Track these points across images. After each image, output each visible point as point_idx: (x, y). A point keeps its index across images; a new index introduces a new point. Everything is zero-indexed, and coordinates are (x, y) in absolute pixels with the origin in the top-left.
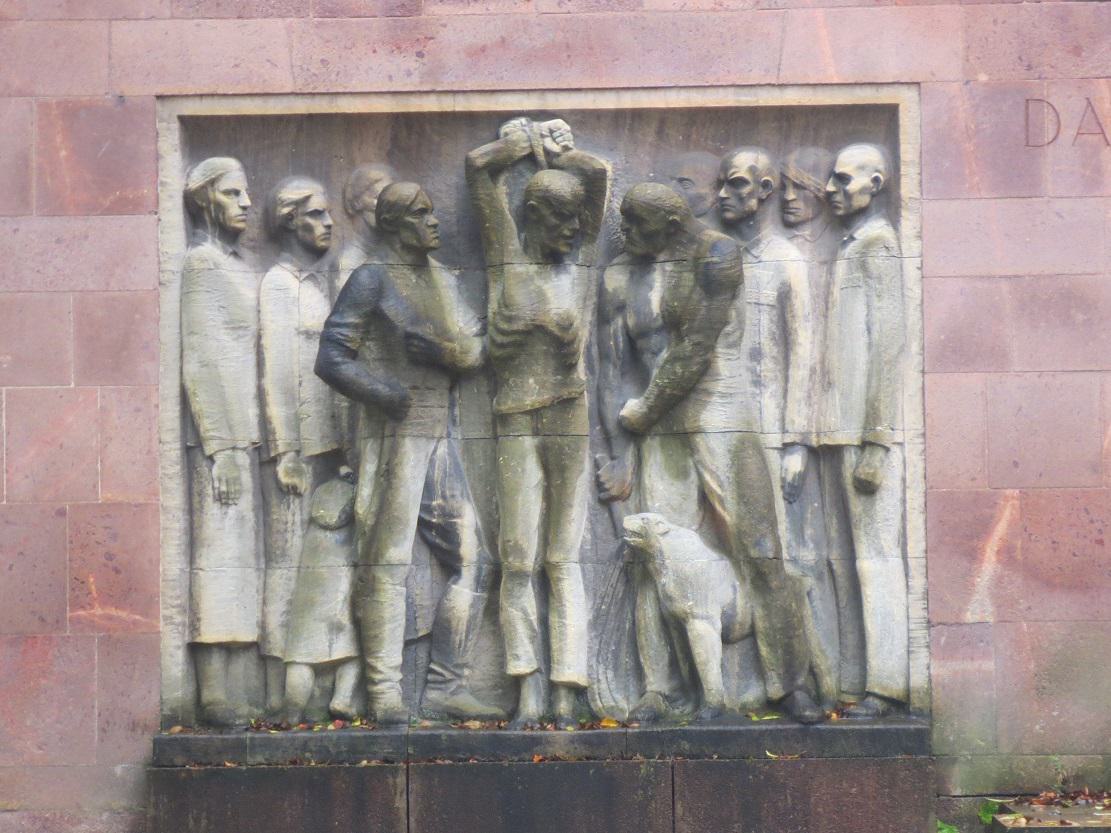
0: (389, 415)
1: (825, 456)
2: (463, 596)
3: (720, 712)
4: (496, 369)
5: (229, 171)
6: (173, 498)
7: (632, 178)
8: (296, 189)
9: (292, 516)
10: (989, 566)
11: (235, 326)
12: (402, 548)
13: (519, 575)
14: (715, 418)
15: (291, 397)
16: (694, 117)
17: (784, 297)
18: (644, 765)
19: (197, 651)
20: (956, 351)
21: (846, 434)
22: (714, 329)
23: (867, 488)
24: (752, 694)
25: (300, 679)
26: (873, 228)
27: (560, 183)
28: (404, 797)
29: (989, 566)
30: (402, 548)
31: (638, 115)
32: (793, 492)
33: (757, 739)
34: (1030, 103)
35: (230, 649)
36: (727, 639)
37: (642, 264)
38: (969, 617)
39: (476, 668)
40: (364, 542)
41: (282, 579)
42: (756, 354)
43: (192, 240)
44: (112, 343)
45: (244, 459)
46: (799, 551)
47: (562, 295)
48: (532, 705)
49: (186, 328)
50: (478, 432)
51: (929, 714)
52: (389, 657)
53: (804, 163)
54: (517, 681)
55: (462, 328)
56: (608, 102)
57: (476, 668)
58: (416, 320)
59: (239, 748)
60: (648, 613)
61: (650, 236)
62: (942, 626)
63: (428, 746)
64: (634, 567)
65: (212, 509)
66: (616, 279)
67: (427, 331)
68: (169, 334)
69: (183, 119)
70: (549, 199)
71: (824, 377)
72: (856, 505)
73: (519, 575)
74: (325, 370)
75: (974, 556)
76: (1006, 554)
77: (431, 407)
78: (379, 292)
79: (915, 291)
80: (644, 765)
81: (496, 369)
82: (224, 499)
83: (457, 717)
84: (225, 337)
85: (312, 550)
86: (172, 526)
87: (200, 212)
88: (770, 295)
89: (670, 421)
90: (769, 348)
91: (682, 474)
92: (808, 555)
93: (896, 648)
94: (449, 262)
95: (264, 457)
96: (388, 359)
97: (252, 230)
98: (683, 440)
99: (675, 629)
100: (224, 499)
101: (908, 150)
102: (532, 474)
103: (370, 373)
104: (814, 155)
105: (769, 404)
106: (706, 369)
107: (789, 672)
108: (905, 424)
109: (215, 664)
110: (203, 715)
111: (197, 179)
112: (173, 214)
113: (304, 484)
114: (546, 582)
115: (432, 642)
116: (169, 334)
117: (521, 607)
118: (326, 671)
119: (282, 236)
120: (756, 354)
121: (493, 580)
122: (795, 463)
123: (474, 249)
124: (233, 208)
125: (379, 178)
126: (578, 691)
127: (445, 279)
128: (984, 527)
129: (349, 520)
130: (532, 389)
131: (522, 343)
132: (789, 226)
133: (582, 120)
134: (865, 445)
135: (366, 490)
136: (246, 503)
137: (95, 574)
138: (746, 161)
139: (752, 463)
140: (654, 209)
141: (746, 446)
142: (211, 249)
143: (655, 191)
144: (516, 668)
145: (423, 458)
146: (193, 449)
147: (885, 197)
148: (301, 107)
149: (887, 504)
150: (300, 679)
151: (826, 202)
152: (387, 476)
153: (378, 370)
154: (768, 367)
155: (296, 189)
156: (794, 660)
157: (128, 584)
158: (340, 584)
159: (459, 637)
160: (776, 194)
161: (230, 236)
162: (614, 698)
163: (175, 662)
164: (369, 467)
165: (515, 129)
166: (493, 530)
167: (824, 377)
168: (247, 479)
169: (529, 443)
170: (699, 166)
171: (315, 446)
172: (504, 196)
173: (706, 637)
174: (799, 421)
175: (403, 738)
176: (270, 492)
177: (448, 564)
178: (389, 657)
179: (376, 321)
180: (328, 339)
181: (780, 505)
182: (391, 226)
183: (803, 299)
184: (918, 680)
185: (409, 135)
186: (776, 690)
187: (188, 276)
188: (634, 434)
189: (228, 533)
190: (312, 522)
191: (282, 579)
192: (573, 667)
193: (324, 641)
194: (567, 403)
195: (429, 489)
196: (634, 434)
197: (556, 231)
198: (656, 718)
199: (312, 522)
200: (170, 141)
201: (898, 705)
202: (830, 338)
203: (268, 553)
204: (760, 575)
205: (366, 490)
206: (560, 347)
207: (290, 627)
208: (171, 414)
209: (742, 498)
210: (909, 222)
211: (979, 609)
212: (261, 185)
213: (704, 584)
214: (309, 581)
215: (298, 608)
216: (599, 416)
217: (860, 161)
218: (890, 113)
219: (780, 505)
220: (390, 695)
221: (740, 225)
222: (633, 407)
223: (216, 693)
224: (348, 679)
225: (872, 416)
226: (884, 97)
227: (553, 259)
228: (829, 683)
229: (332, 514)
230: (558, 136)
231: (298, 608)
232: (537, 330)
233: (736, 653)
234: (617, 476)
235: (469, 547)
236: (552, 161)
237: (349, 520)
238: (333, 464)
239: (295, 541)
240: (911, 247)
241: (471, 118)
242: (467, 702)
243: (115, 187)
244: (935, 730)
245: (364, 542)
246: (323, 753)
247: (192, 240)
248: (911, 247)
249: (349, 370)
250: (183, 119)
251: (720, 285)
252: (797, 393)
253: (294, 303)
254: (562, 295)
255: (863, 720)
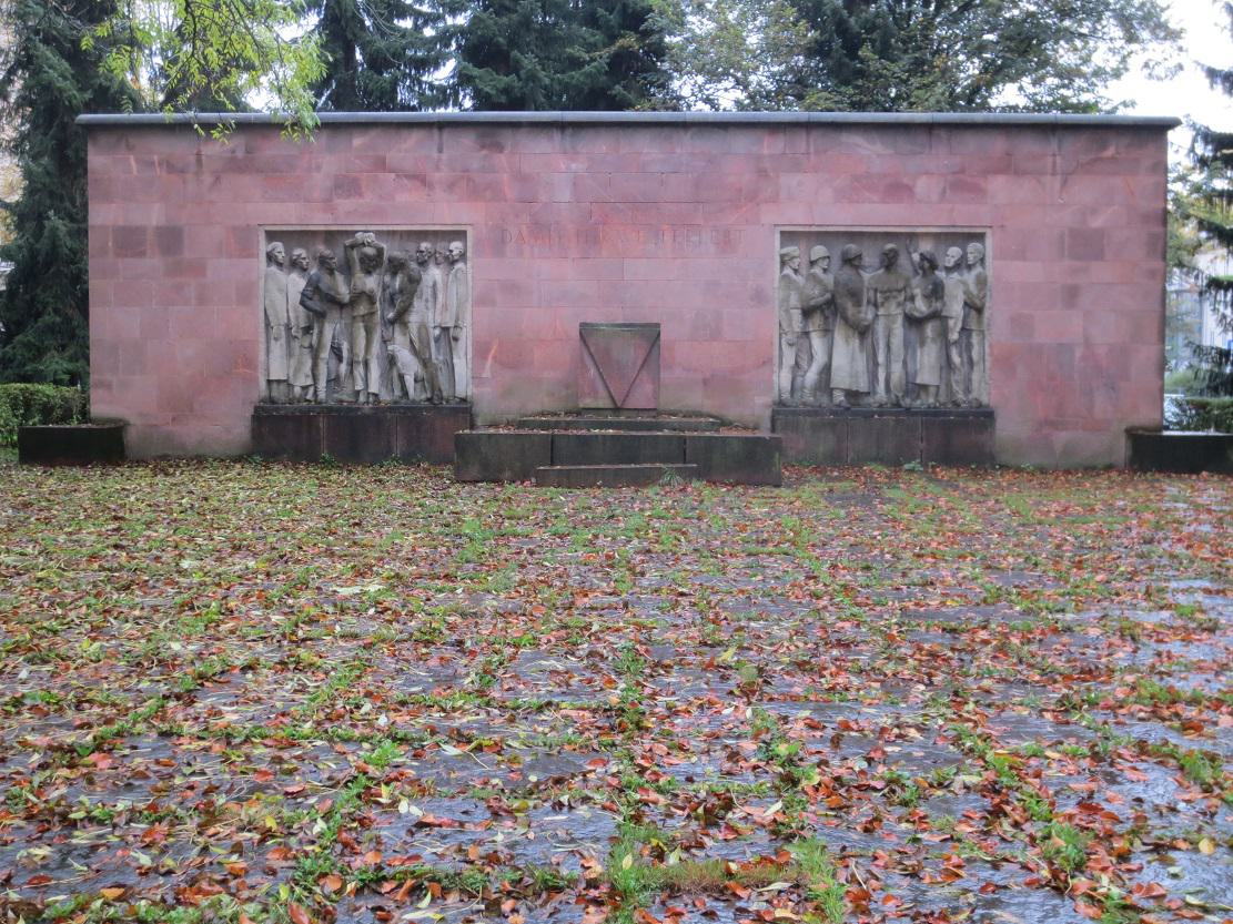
0: (321, 316)
1: (445, 330)
2: (343, 368)
3: (414, 401)
4: (353, 303)
5: (279, 246)
6: (262, 339)
7: (391, 250)
8: (298, 251)
9: (296, 345)
10: (490, 360)
11: (280, 290)
12: (325, 354)
13: (358, 362)
14: (413, 319)
15: (295, 311)
16: (410, 234)
17: (435, 284)
18: (389, 415)
19: (269, 382)
20: (482, 301)
21: (451, 324)
22: (412, 294)
23: (456, 339)
24: (423, 397)
25: (297, 390)
26: (460, 265)
27: (370, 251)
28: (322, 423)
29: (490, 360)
30: (325, 354)
31: (394, 232)
32: (437, 340)
33: (421, 409)
34: (503, 231)
35: (279, 382)
36: (416, 381)
37: (394, 274)
38: (484, 375)
39: (348, 389)
40: (315, 352)
41: (293, 362)
42: (427, 301)
43: (268, 266)
44: (246, 294)
45: (283, 328)
46: (437, 356)
47: (371, 283)
48: (362, 398)
49: (266, 291)
50: (348, 321)
51: (472, 403)
52: (322, 384)
53: (441, 246)
54: (358, 392)
55: (344, 292)
56: (385, 228)
57: (348, 389)
58: (330, 289)
59: (277, 409)
60: (395, 374)
61: (396, 267)
62: (476, 378)
63: (330, 409)
64: (391, 361)
65: (273, 342)
66: (387, 278)
67: (332, 293)
68: (261, 293)
69: (267, 232)
70: (366, 255)
71: (445, 307)
72: (453, 343)
73: (358, 362)
74: (302, 303)
75: (486, 358)
76: (494, 358)
77: (334, 314)
78: (318, 281)
79: (470, 284)
80: (389, 415)
81: (353, 303)
82: (276, 339)
83: (341, 401)
84: (277, 294)
85: (301, 354)
86: (262, 347)
87: (271, 258)
88: (431, 284)
89: (400, 319)
90: (430, 299)
91: (405, 335)
92: (441, 358)
93: (463, 385)
94: (342, 273)
95: (288, 328)
96: (321, 300)
97: (287, 263)
98: (405, 325)
99: (401, 377)
100: (276, 339)
101: (469, 244)
102: (362, 333)
103: (316, 304)
104: (444, 244)
105: (430, 315)
106: (411, 304)
107: (433, 392)
108: (467, 322)
109: (275, 385)
110: (272, 401)
111: (270, 248)
112: (263, 258)
113: (299, 335)
114: (366, 364)
115: (334, 381)
116: (261, 293)
117: (359, 371)
118: (305, 388)
119: (295, 265)
120: (427, 301)
121: (351, 364)
122: (437, 332)
123: (347, 269)
124: (280, 257)
125: (322, 249)
126: (376, 395)
127: (340, 278)
128: (488, 351)
129: (311, 346)
130: (362, 309)
131: (360, 296)
132: (438, 264)
133: (378, 233)
134: (456, 327)
135: (315, 337)
136: (283, 340)
137: (241, 360)
138: (424, 245)
139: (423, 331)
140: (395, 259)
141: (423, 327)
142: (274, 268)
143: (397, 254)
144: (358, 388)
145: (330, 329)
146: (268, 325)
147: (463, 256)
148: (299, 228)
149: (461, 343)
150: (297, 390)
151: (447, 258)
152: (321, 332)
153: (319, 303)
154: (430, 304)
155: (298, 251)
156: (434, 387)
157: (250, 363)
158: (309, 363)
159: (342, 379)
160: (433, 255)
161: (280, 265)
162: (385, 397)
163: (263, 384)
164: (316, 331)
165: (359, 235)
166: (351, 350)
167: (445, 307)
168: (283, 333)
169: (361, 324)
170: (411, 247)
171: (303, 325)
172: (355, 254)
173: (410, 381)
174: (438, 320)
175: (399, 446)
176: (290, 338)
177: (340, 359)
178: (322, 384)
179: (317, 289)
180: (303, 294)
181: (433, 344)
182: (323, 262)
183: (440, 285)
184: (469, 393)
185: (330, 236)
186: (429, 395)
187: (267, 276)
188: (392, 322)
189: (278, 349)
190: (301, 346)
191: (293, 362)
192: (374, 388)
193: (304, 380)
194: (373, 314)
195: (334, 338)
196: (392, 322)
197: (371, 264)
198: (396, 402)
199: (301, 346)
200: (262, 237)
201: (464, 400)
202: (446, 296)
203: (290, 354)
204: (425, 363)
205: (315, 337)
206: (371, 299)
207: (294, 375)
208: (262, 314)
209: (421, 341)
210: (469, 264)
211: (487, 374)
212: (288, 251)
213: (409, 364)
214: (300, 363)
215: (297, 370)
216: (383, 317)
217: (456, 246)
218: (465, 232)
219: (433, 344)
220: (322, 395)
221: (423, 264)
222: (391, 315)
223: (275, 394)
224: (311, 390)
225: (457, 319)
226: (463, 228)
227: (369, 273)
228: (445, 394)
229: (306, 344)
230: (371, 238)
231: (297, 370)
232: (363, 293)
233: (419, 386)
234: (387, 335)
235: (345, 354)
236: (369, 245)
237: (311, 346)
238: (307, 330)
239: (297, 351)
240: (470, 271)
241: (347, 232)
242: (345, 397)
243: (247, 251)
244: (93, 241)
245: (315, 352)
246: (300, 411)
247: (268, 266)
248: (470, 271)
249: (309, 303)
250: (267, 232)
251: (414, 281)
252: (438, 312)
253: (297, 283)
254: (371, 283)
255: (453, 404)
